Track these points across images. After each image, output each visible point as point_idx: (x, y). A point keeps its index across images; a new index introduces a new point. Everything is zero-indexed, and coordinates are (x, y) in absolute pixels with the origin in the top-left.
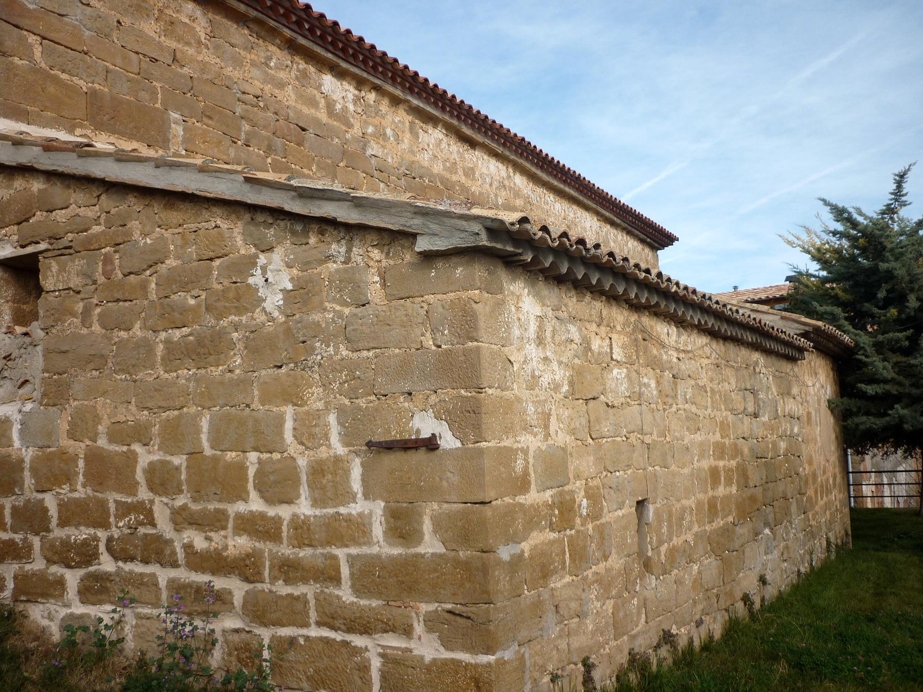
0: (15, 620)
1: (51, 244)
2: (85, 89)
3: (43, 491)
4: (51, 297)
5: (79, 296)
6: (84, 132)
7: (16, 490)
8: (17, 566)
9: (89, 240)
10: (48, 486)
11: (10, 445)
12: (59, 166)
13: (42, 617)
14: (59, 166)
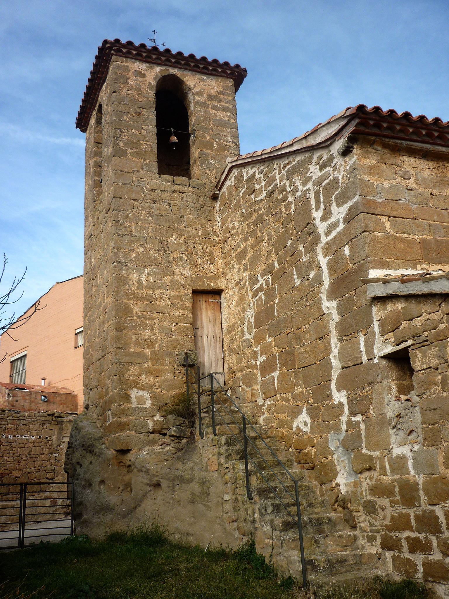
0: (427, 595)
1: (415, 341)
2: (418, 240)
3: (433, 505)
4: (420, 375)
5: (437, 372)
6: (422, 266)
7: (416, 503)
8: (423, 556)
9: (438, 334)
10: (435, 501)
11: (408, 473)
12: (412, 291)
13: (445, 594)
14: (412, 291)
